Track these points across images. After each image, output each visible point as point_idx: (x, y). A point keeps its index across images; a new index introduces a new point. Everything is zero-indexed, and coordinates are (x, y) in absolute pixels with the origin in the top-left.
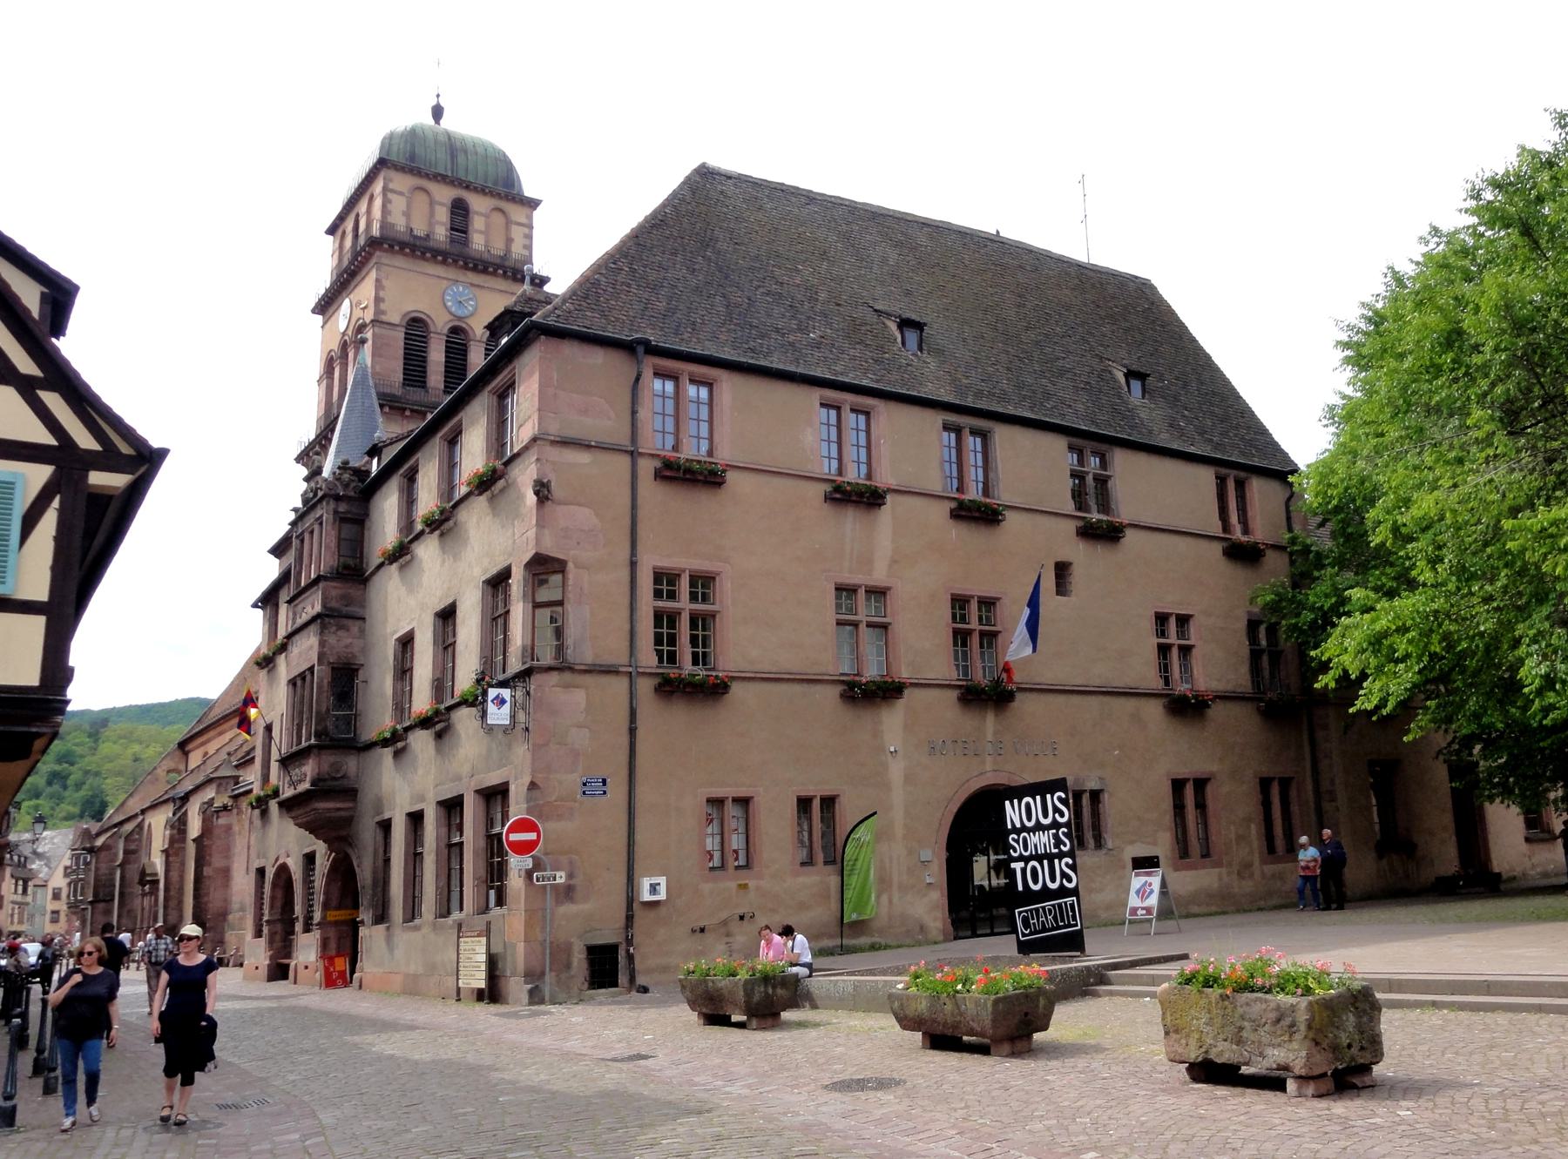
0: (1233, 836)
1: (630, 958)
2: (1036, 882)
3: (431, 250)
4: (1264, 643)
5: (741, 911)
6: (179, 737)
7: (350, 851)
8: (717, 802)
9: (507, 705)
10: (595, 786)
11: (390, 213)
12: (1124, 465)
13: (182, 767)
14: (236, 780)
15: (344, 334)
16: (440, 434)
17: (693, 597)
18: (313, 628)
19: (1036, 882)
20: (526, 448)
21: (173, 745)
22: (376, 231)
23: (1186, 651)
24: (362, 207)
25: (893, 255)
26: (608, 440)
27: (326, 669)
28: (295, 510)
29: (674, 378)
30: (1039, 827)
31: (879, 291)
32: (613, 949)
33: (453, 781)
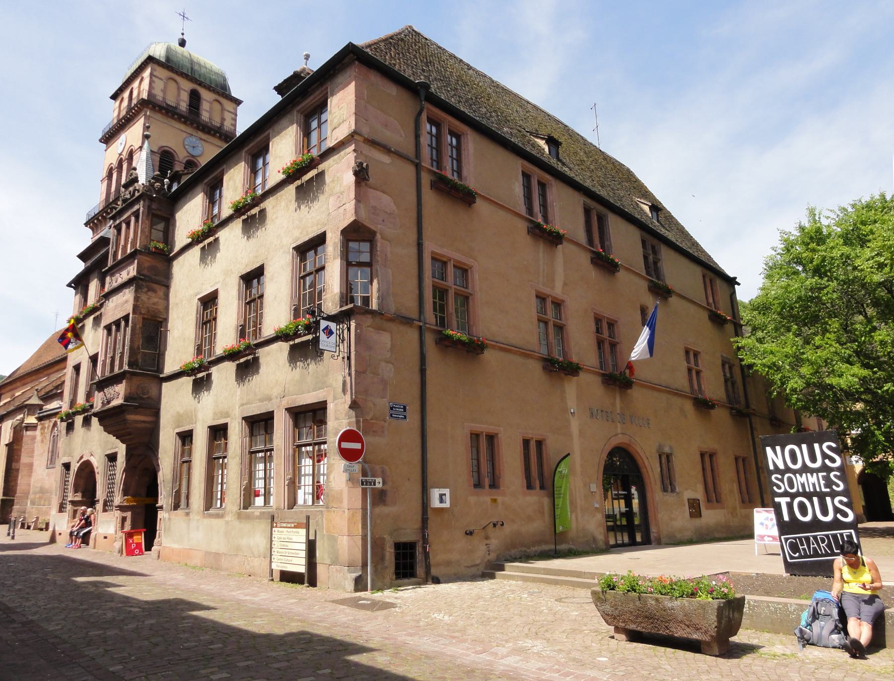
1: (426, 555)
2: (804, 514)
3: (177, 114)
5: (494, 520)
10: (397, 411)
15: (120, 154)
16: (246, 149)
19: (804, 514)
22: (145, 96)
23: (698, 373)
24: (136, 84)
27: (139, 318)
30: (805, 469)
32: (411, 546)
33: (261, 400)
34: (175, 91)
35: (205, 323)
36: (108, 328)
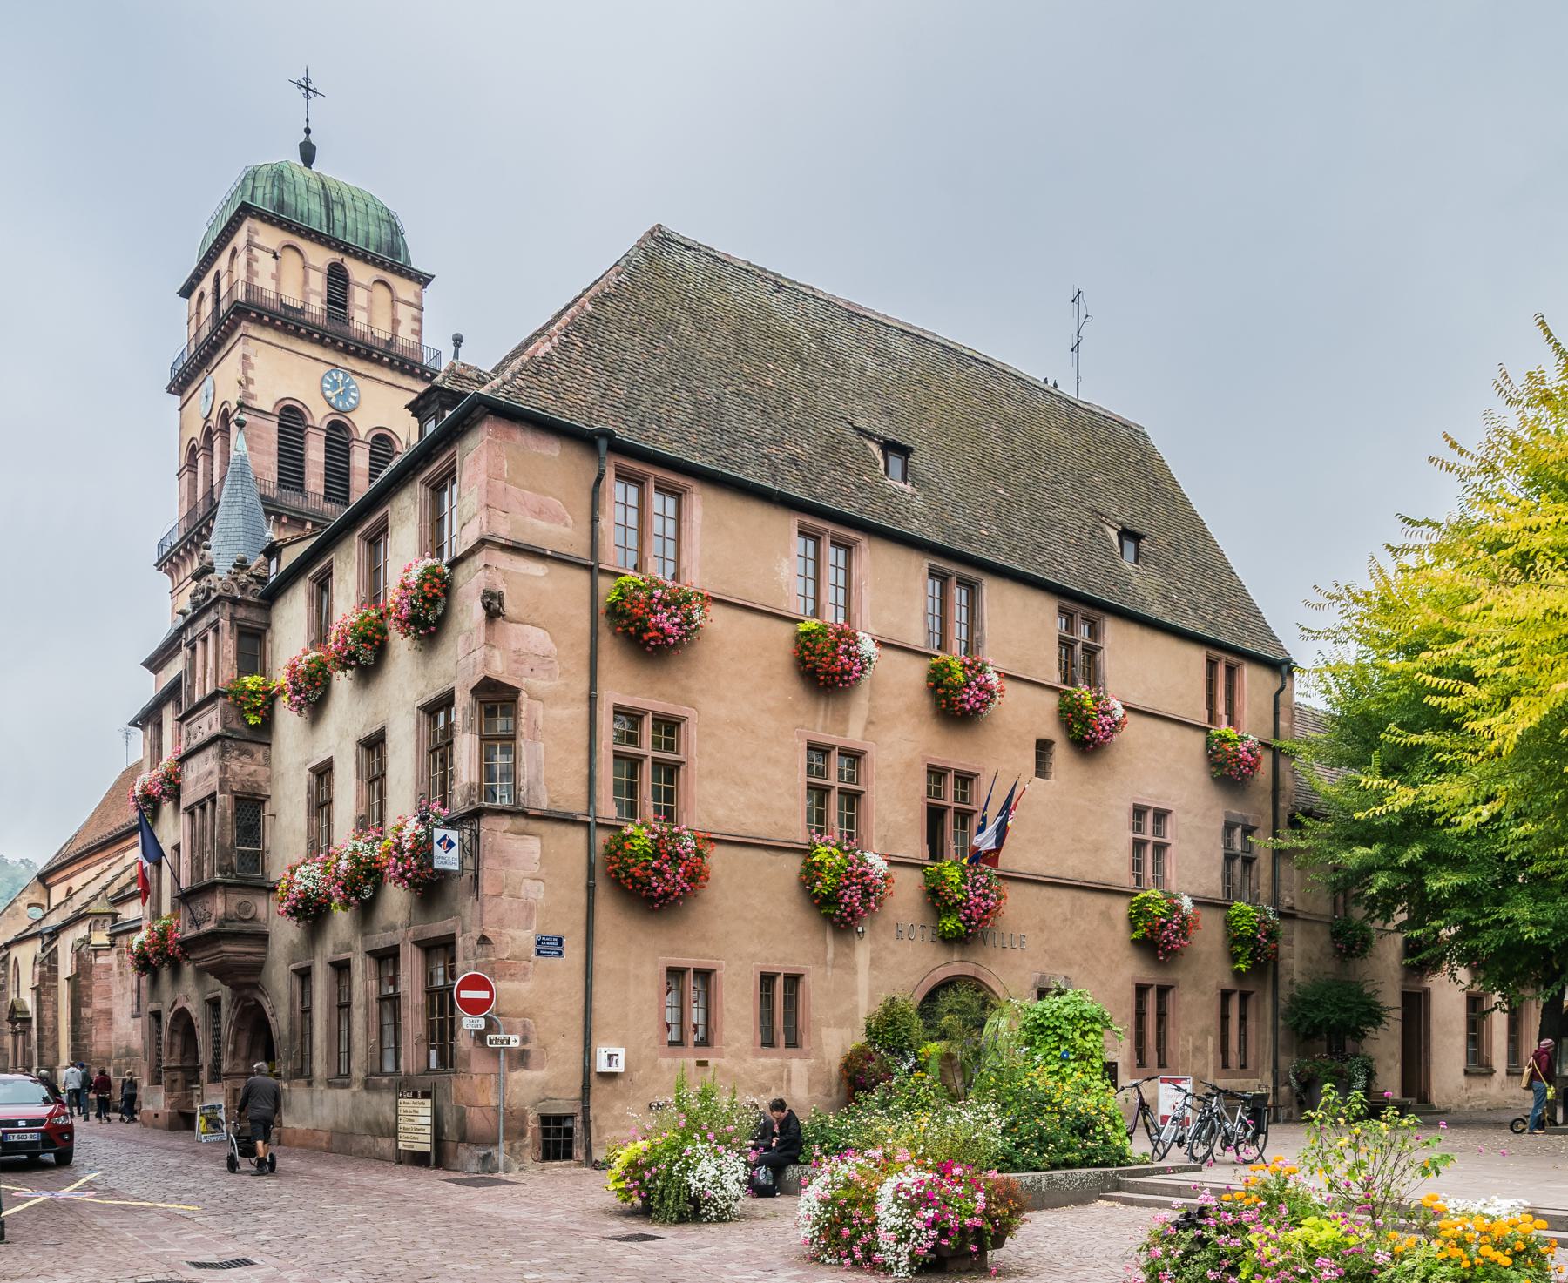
0: (1190, 1047)
4: (1238, 847)
6: (41, 864)
7: (261, 999)
8: (675, 973)
9: (456, 848)
10: (549, 946)
11: (256, 274)
12: (1117, 639)
13: (45, 902)
14: (114, 915)
16: (360, 532)
17: (656, 744)
18: (212, 751)
20: (471, 552)
21: (29, 877)
22: (240, 294)
23: (1160, 848)
24: (222, 263)
25: (871, 363)
26: (564, 550)
28: (183, 613)
29: (638, 481)
31: (857, 405)
34: (299, 272)
35: (320, 806)
36: (190, 811)
